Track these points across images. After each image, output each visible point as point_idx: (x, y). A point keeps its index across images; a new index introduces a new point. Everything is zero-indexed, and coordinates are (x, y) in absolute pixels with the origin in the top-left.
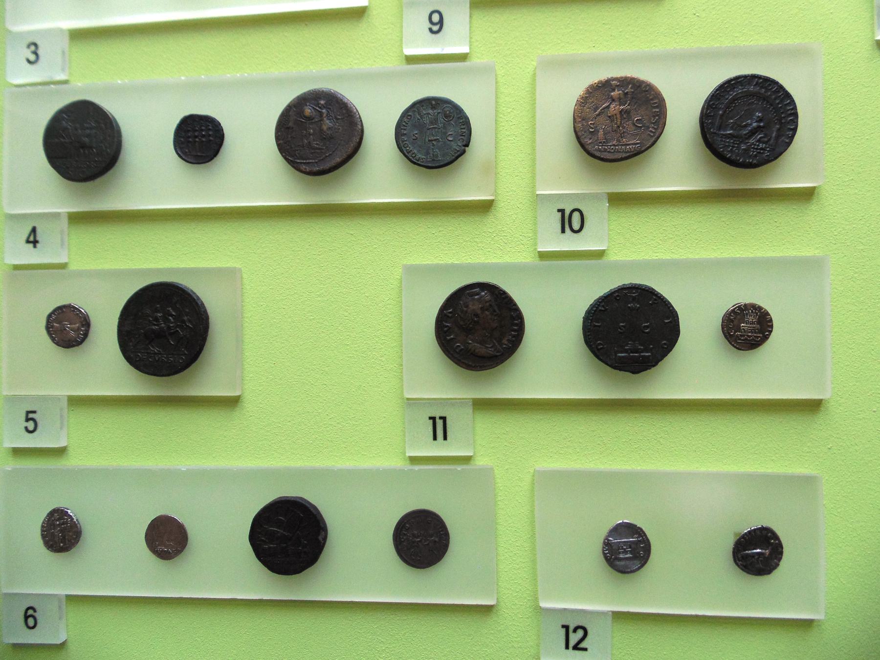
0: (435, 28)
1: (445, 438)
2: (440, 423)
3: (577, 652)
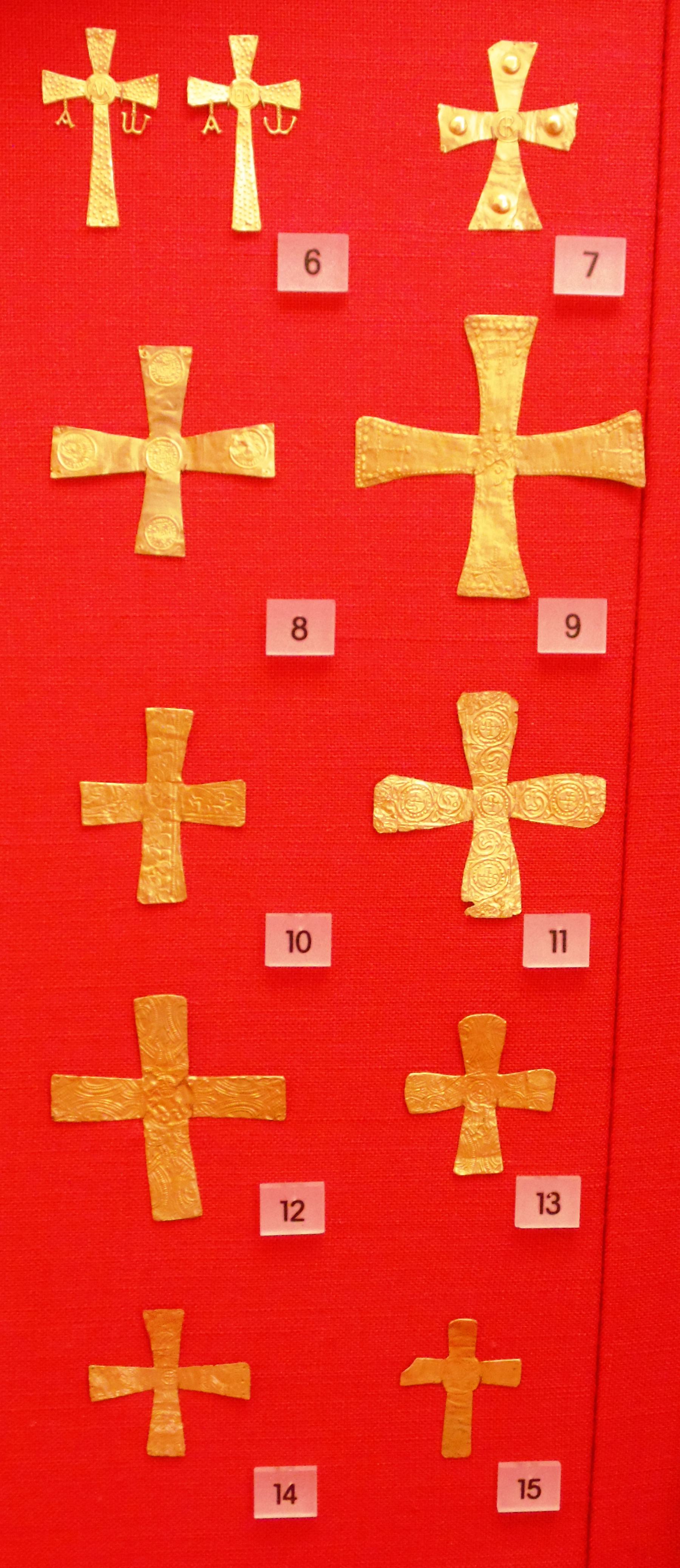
0: (573, 632)
1: (564, 950)
2: (560, 937)
3: (295, 1223)
